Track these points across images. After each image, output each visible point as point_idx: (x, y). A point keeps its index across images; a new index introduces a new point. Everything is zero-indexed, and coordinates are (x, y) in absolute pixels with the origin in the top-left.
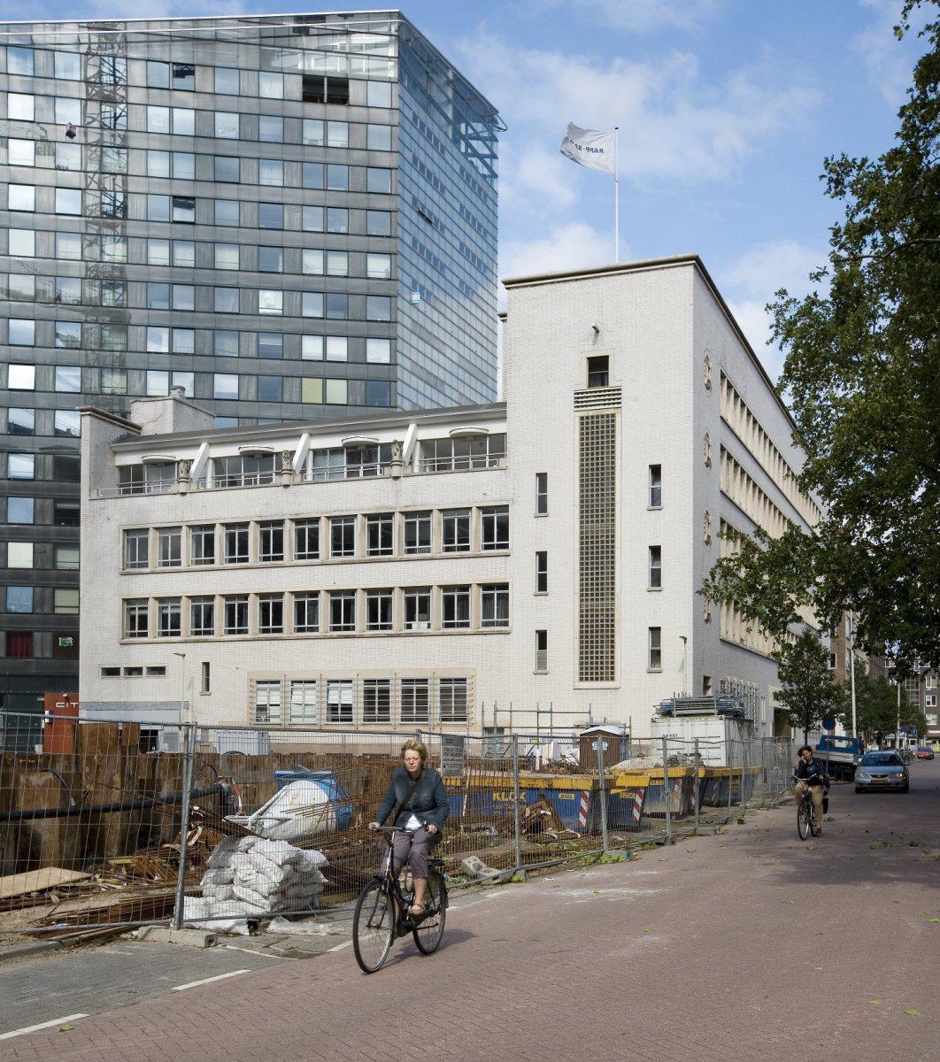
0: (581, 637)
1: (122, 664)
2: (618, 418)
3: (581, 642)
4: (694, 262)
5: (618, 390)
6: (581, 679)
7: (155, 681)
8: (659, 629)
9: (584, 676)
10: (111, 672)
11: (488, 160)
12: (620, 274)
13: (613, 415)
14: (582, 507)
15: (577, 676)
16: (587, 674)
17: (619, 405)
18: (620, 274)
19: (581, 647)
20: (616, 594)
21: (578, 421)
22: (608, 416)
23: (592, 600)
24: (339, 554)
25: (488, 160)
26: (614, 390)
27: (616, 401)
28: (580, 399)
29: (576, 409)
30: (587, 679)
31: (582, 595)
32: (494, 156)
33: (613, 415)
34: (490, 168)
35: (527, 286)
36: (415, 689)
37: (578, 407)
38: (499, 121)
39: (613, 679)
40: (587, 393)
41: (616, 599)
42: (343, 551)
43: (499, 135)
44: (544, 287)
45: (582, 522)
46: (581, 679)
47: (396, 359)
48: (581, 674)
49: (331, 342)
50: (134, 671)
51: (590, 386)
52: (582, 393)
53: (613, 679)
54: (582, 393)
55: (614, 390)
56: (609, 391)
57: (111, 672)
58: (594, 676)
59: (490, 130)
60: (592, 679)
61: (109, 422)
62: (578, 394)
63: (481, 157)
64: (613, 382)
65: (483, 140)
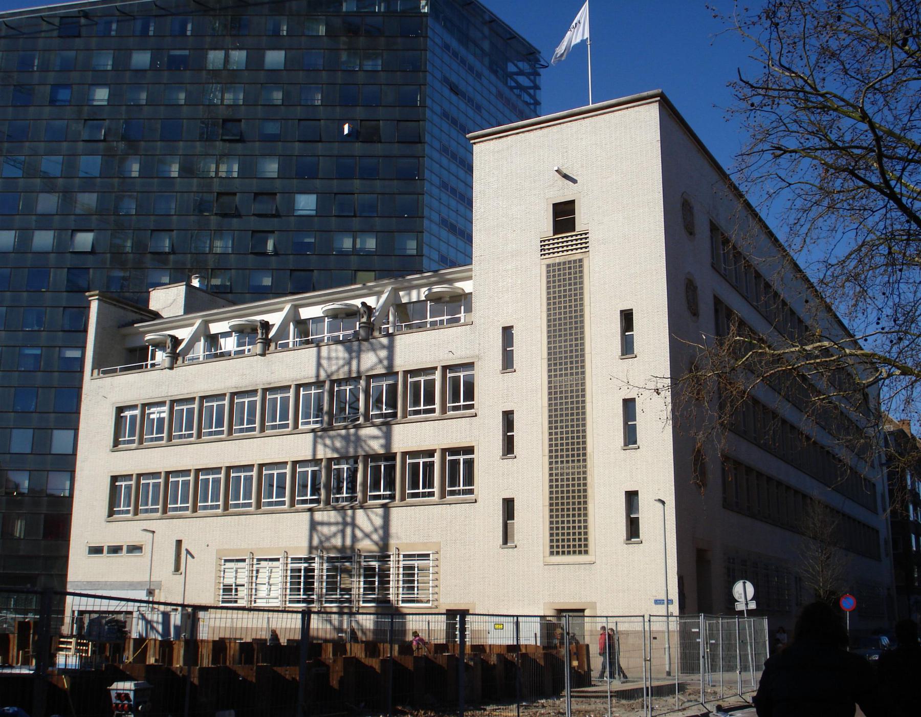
0: (551, 505)
1: (106, 543)
2: (586, 263)
3: (551, 511)
4: (659, 98)
5: (586, 234)
6: (552, 553)
7: (133, 558)
8: (512, 412)
9: (555, 550)
10: (96, 550)
11: (532, 91)
12: (584, 118)
13: (581, 260)
14: (549, 360)
15: (548, 550)
16: (558, 547)
17: (587, 250)
18: (584, 118)
19: (551, 517)
20: (588, 455)
21: (544, 269)
22: (575, 261)
23: (562, 462)
24: (309, 423)
25: (532, 91)
26: (581, 235)
27: (584, 245)
28: (545, 248)
29: (543, 257)
30: (558, 553)
31: (551, 457)
32: (536, 87)
33: (581, 260)
34: (533, 97)
35: (492, 139)
36: (303, 568)
37: (544, 255)
38: (541, 60)
39: (586, 552)
40: (553, 239)
41: (588, 460)
42: (312, 420)
43: (542, 71)
44: (509, 138)
45: (550, 377)
46: (552, 553)
47: (422, 250)
48: (552, 547)
49: (214, 173)
50: (115, 550)
51: (555, 234)
52: (549, 240)
53: (586, 552)
54: (549, 240)
55: (581, 235)
56: (576, 235)
57: (96, 550)
58: (566, 550)
59: (533, 67)
60: (563, 553)
61: (120, 307)
62: (544, 241)
63: (524, 89)
64: (579, 227)
65: (528, 75)
